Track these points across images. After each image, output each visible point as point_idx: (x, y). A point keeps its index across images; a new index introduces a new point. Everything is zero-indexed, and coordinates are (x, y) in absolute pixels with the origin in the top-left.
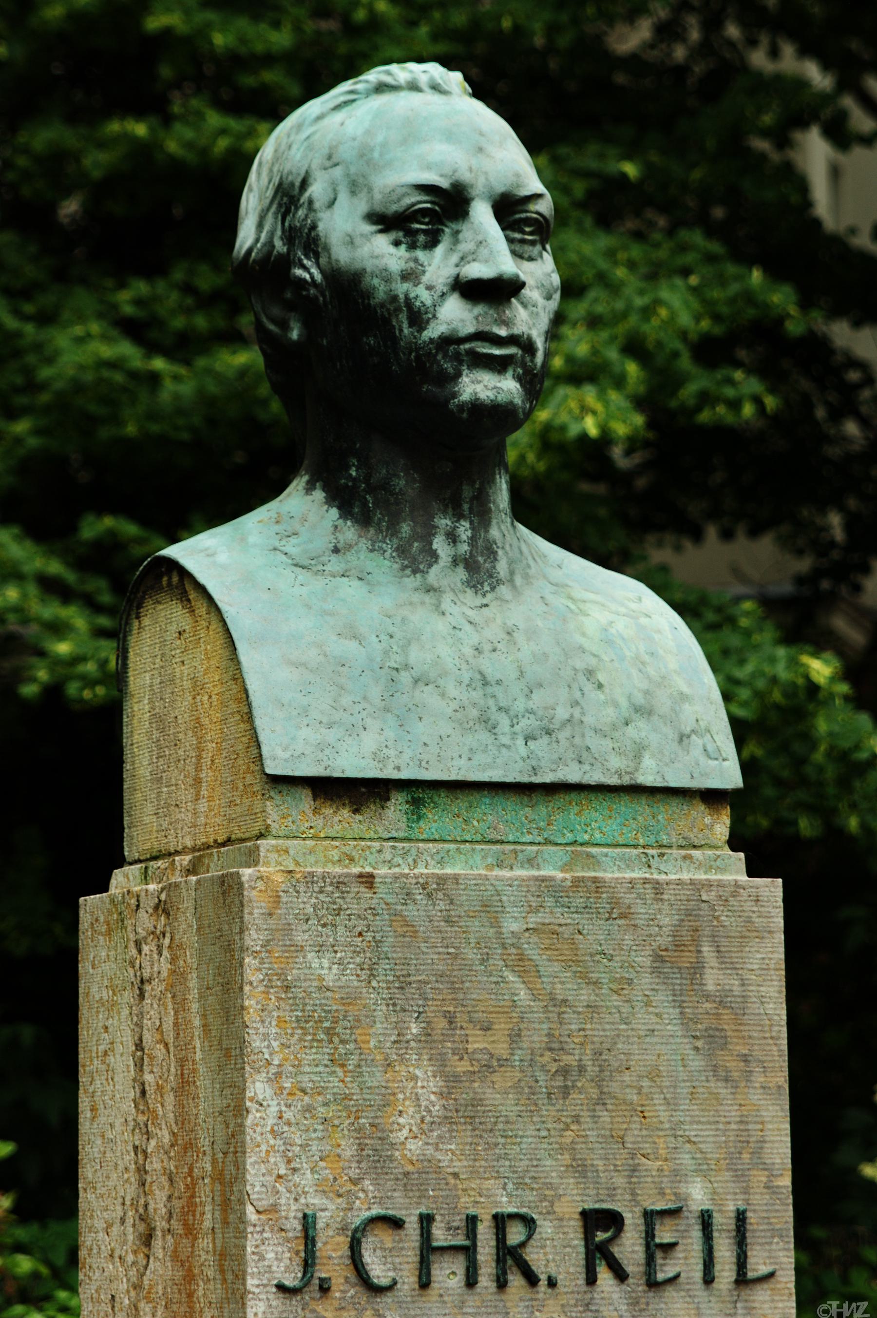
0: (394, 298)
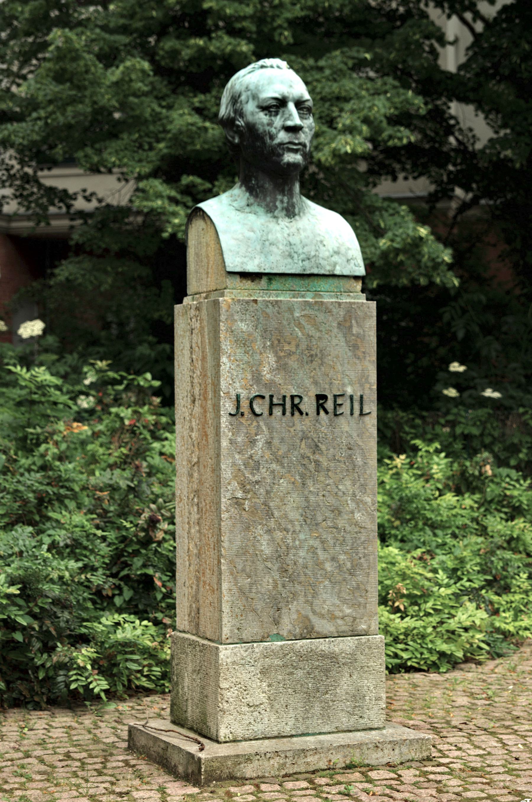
0: (265, 131)
